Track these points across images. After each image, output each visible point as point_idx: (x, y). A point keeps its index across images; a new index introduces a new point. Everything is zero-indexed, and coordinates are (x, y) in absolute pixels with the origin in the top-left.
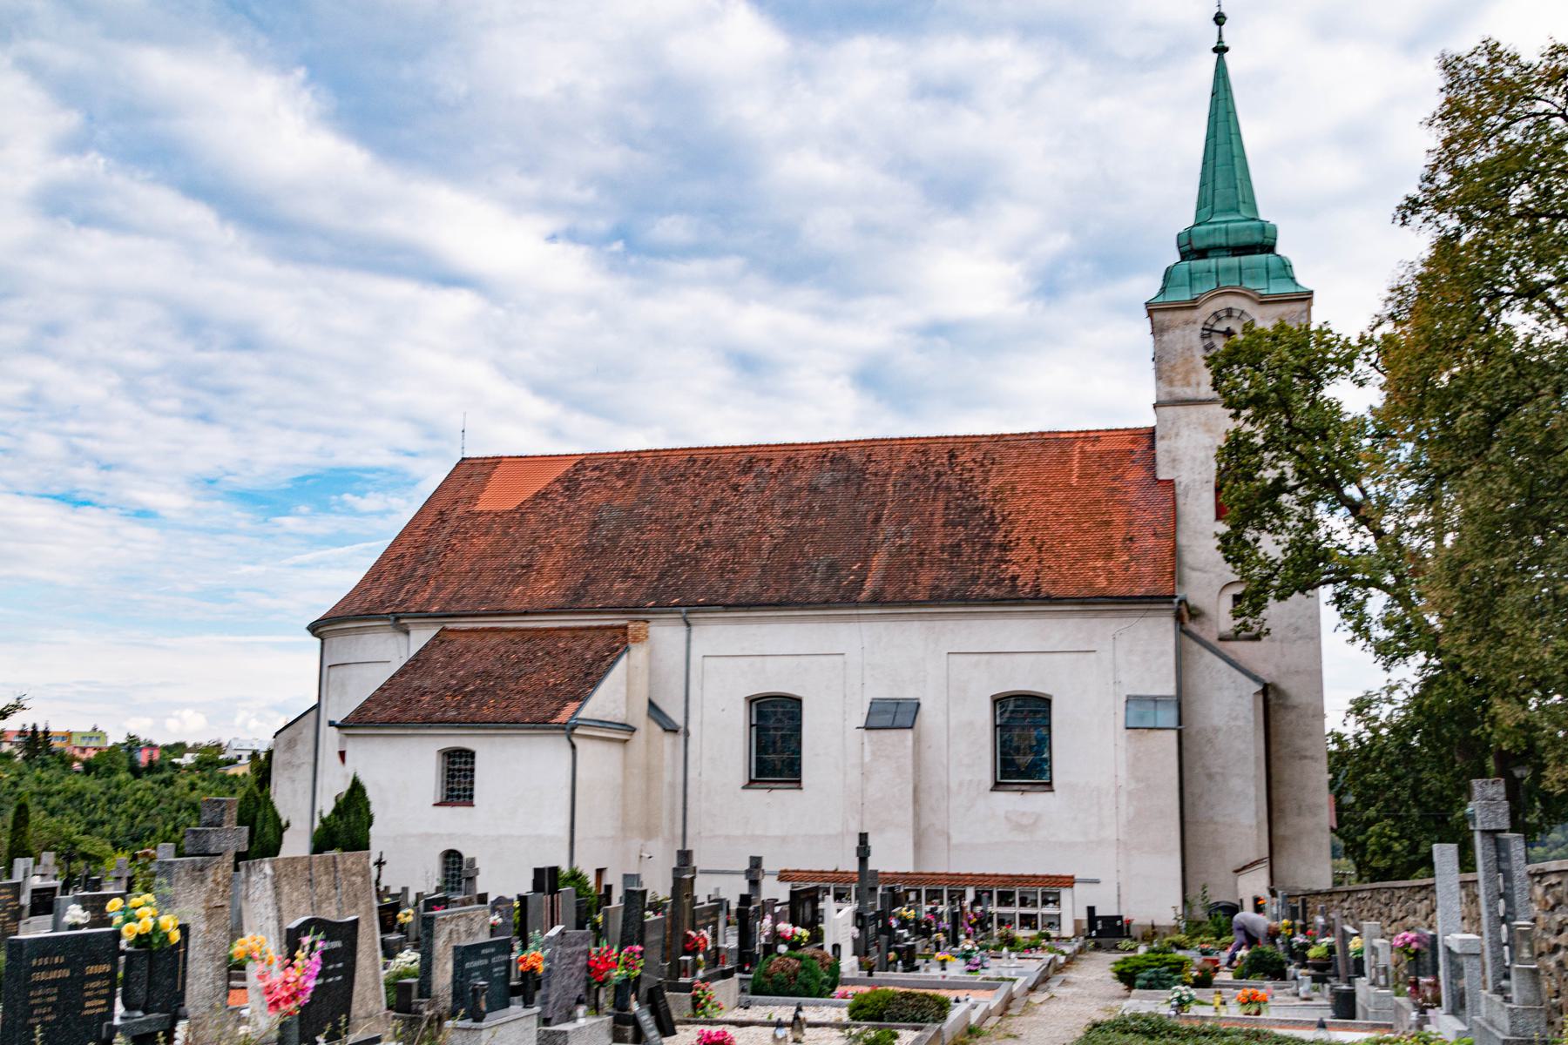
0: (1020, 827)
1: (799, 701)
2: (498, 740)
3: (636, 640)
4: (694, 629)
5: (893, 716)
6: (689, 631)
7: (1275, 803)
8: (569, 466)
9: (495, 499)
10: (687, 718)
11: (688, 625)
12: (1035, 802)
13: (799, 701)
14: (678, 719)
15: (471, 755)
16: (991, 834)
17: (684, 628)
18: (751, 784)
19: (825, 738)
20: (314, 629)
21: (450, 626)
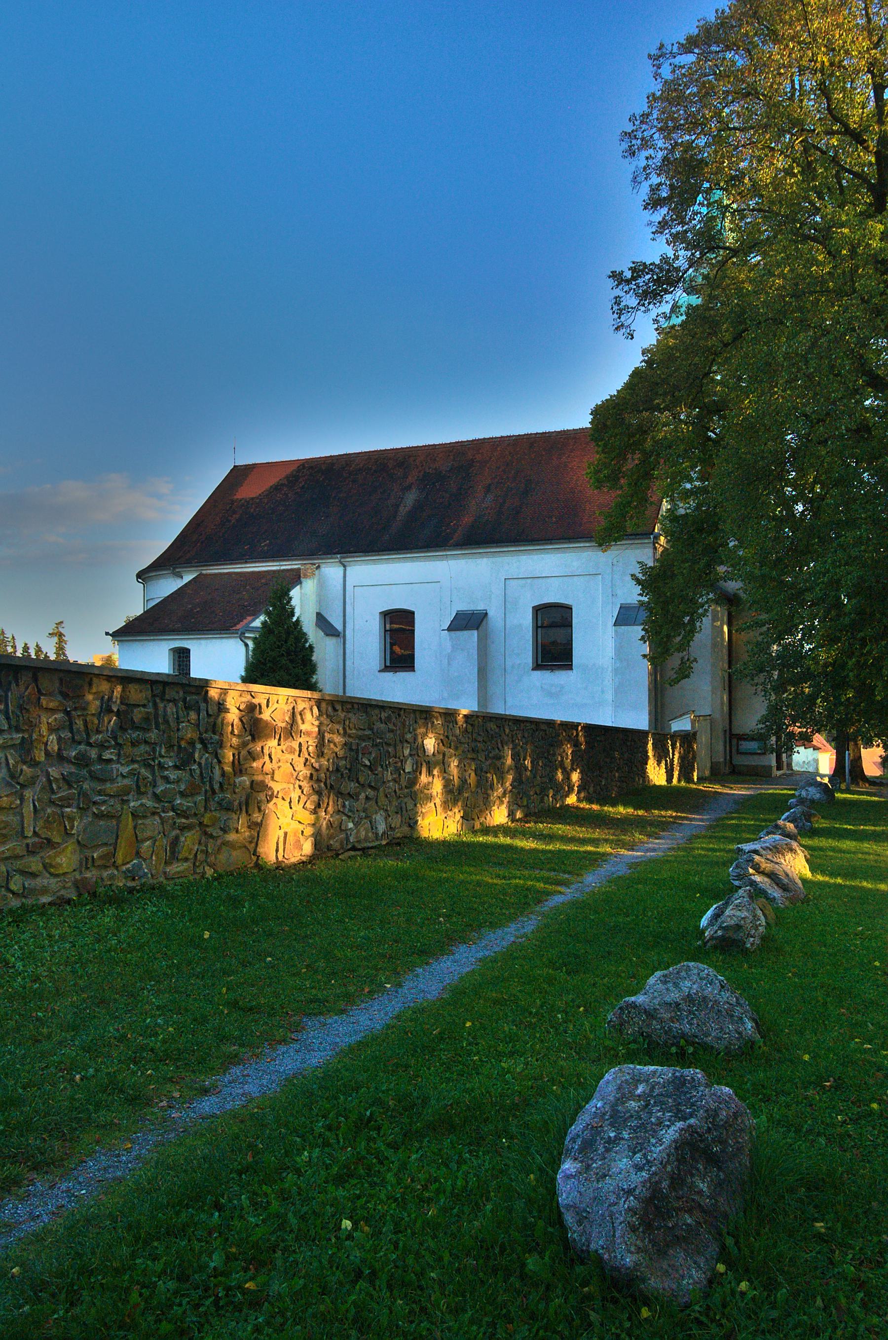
0: (551, 695)
1: (569, 608)
2: (203, 642)
3: (306, 576)
4: (348, 569)
5: (469, 621)
6: (345, 570)
7: (734, 654)
8: (295, 467)
9: (249, 491)
10: (344, 626)
11: (345, 566)
12: (560, 678)
13: (413, 613)
14: (339, 626)
15: (187, 651)
16: (536, 696)
17: (342, 568)
18: (386, 669)
19: (428, 636)
20: (140, 575)
21: (204, 572)
